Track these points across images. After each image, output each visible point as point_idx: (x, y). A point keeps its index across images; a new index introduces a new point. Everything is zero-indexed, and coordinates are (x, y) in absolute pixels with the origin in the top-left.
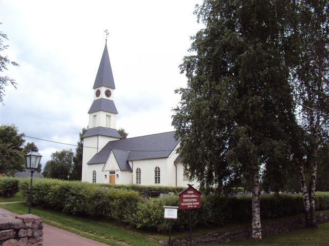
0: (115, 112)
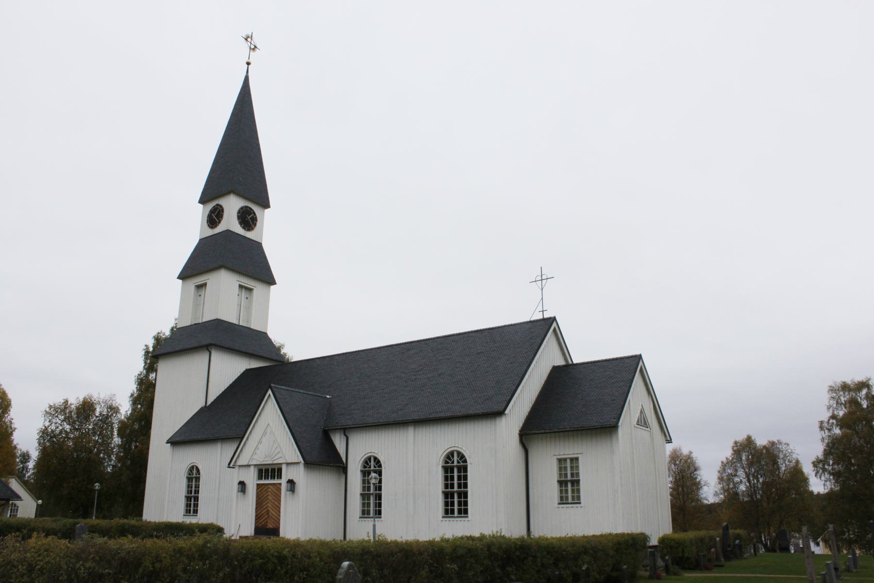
0: (268, 280)
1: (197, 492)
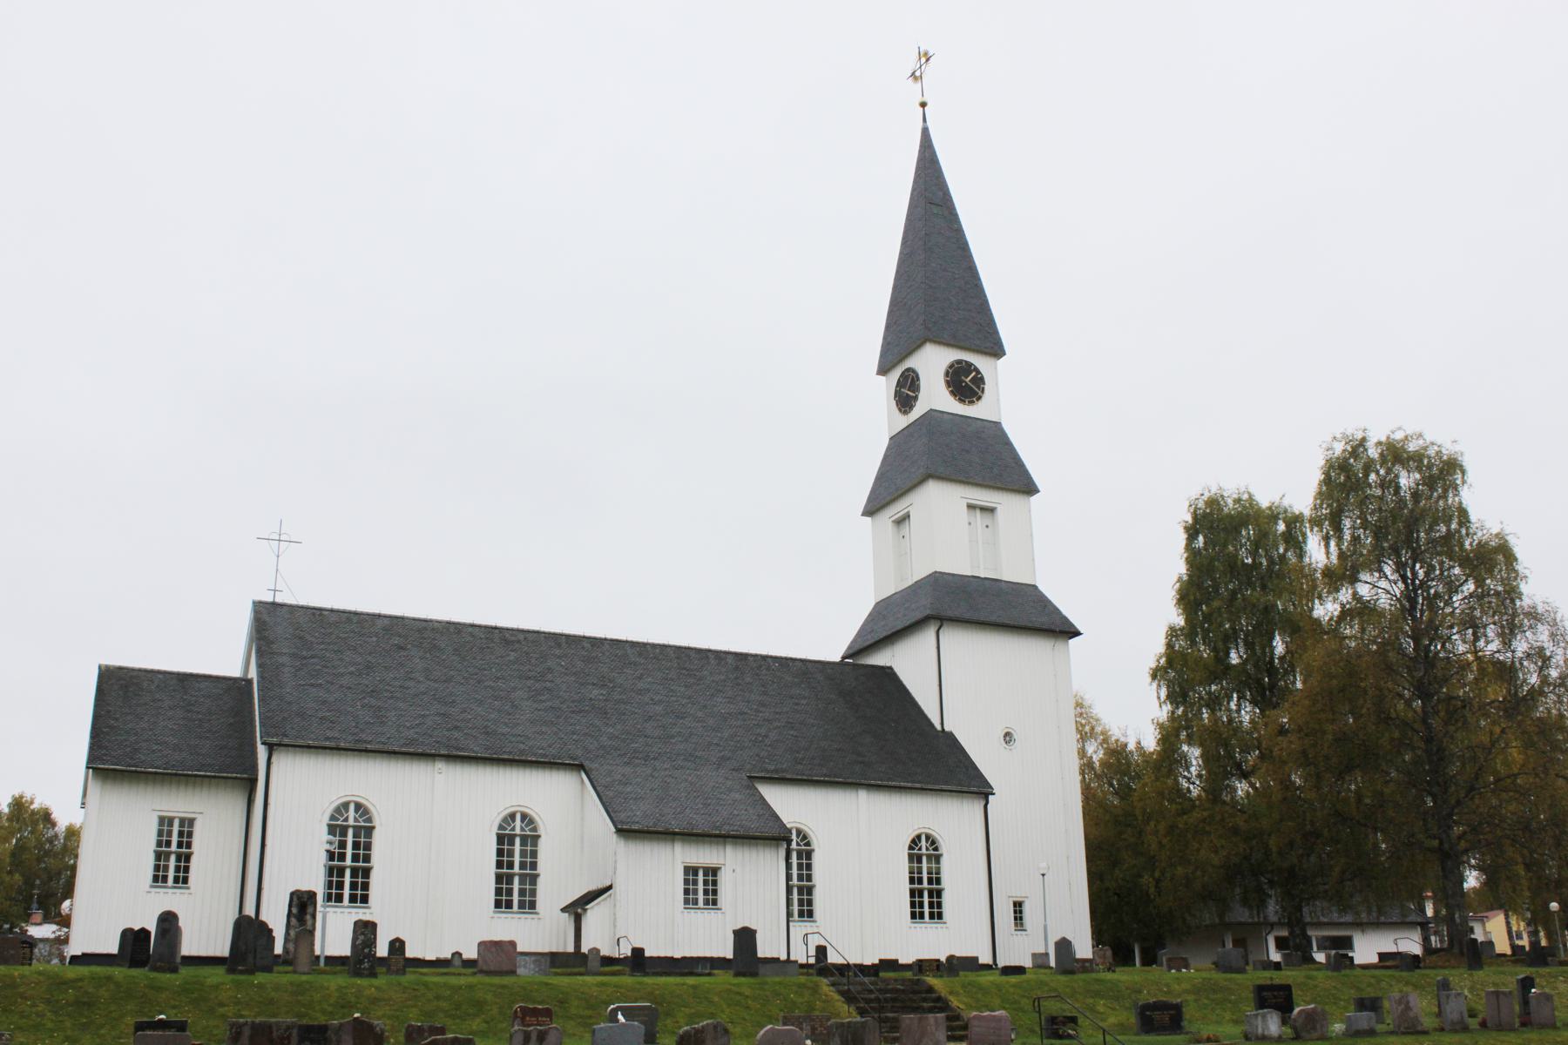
0: (1027, 488)
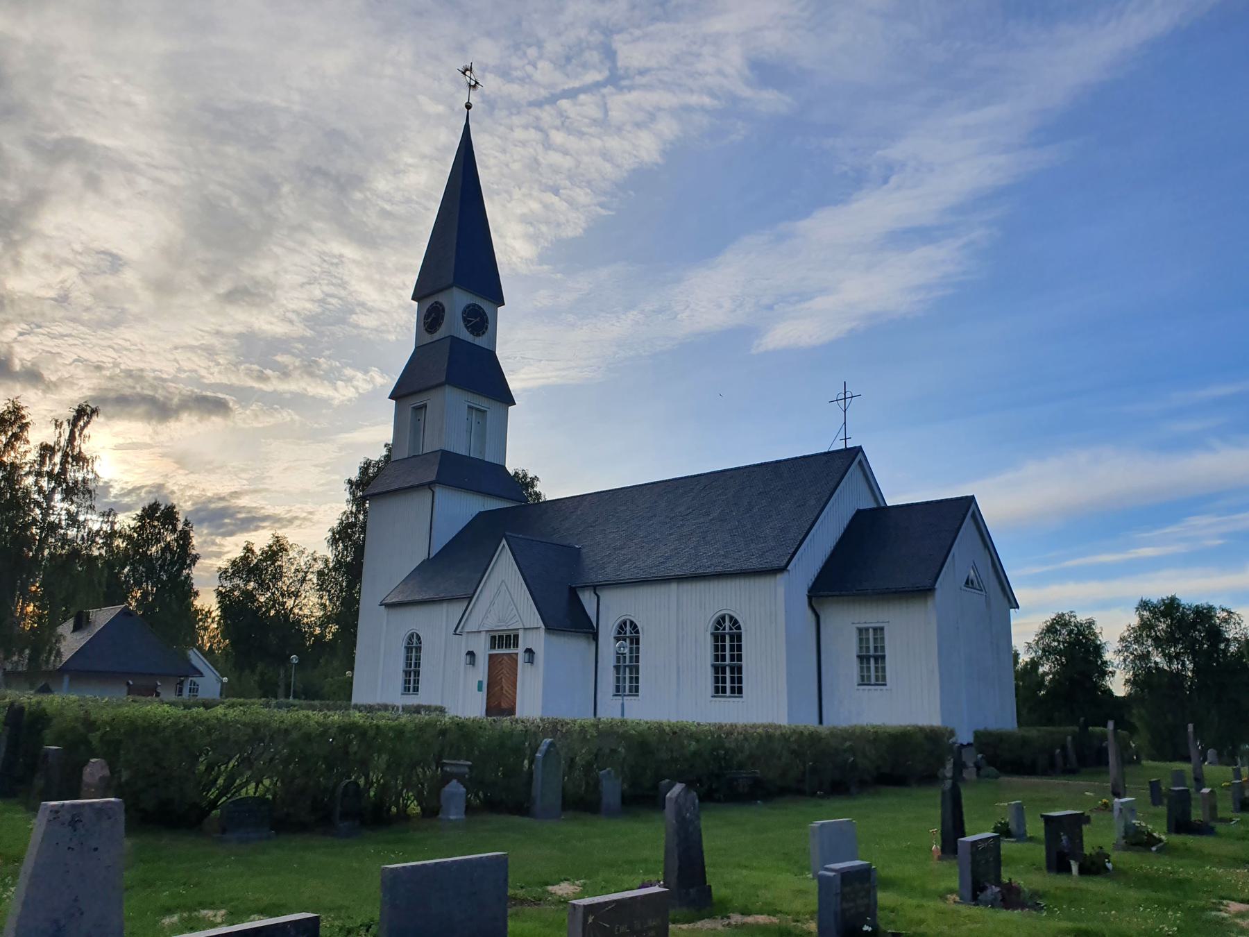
1: (418, 665)
